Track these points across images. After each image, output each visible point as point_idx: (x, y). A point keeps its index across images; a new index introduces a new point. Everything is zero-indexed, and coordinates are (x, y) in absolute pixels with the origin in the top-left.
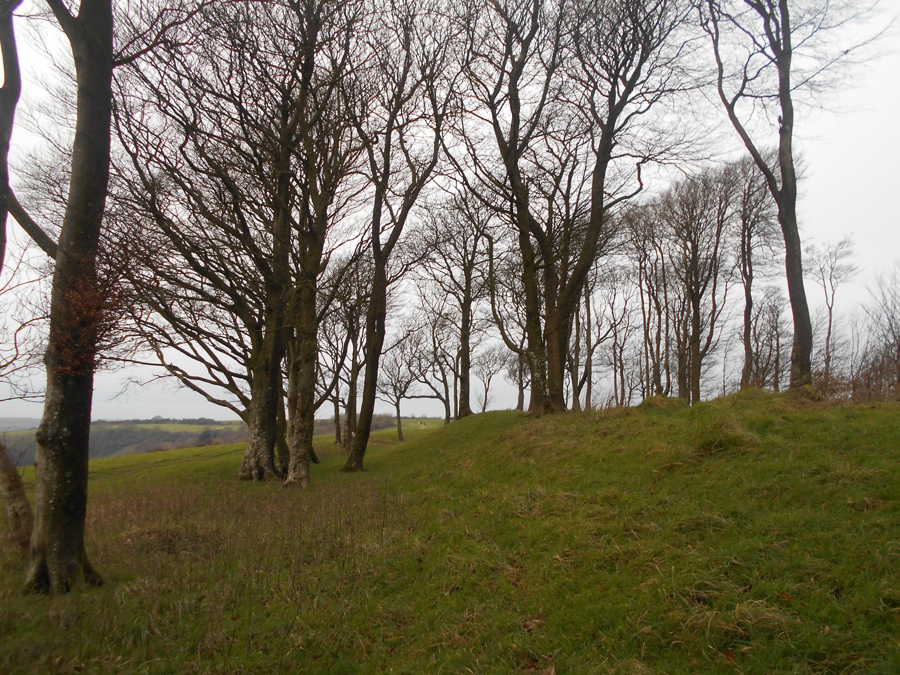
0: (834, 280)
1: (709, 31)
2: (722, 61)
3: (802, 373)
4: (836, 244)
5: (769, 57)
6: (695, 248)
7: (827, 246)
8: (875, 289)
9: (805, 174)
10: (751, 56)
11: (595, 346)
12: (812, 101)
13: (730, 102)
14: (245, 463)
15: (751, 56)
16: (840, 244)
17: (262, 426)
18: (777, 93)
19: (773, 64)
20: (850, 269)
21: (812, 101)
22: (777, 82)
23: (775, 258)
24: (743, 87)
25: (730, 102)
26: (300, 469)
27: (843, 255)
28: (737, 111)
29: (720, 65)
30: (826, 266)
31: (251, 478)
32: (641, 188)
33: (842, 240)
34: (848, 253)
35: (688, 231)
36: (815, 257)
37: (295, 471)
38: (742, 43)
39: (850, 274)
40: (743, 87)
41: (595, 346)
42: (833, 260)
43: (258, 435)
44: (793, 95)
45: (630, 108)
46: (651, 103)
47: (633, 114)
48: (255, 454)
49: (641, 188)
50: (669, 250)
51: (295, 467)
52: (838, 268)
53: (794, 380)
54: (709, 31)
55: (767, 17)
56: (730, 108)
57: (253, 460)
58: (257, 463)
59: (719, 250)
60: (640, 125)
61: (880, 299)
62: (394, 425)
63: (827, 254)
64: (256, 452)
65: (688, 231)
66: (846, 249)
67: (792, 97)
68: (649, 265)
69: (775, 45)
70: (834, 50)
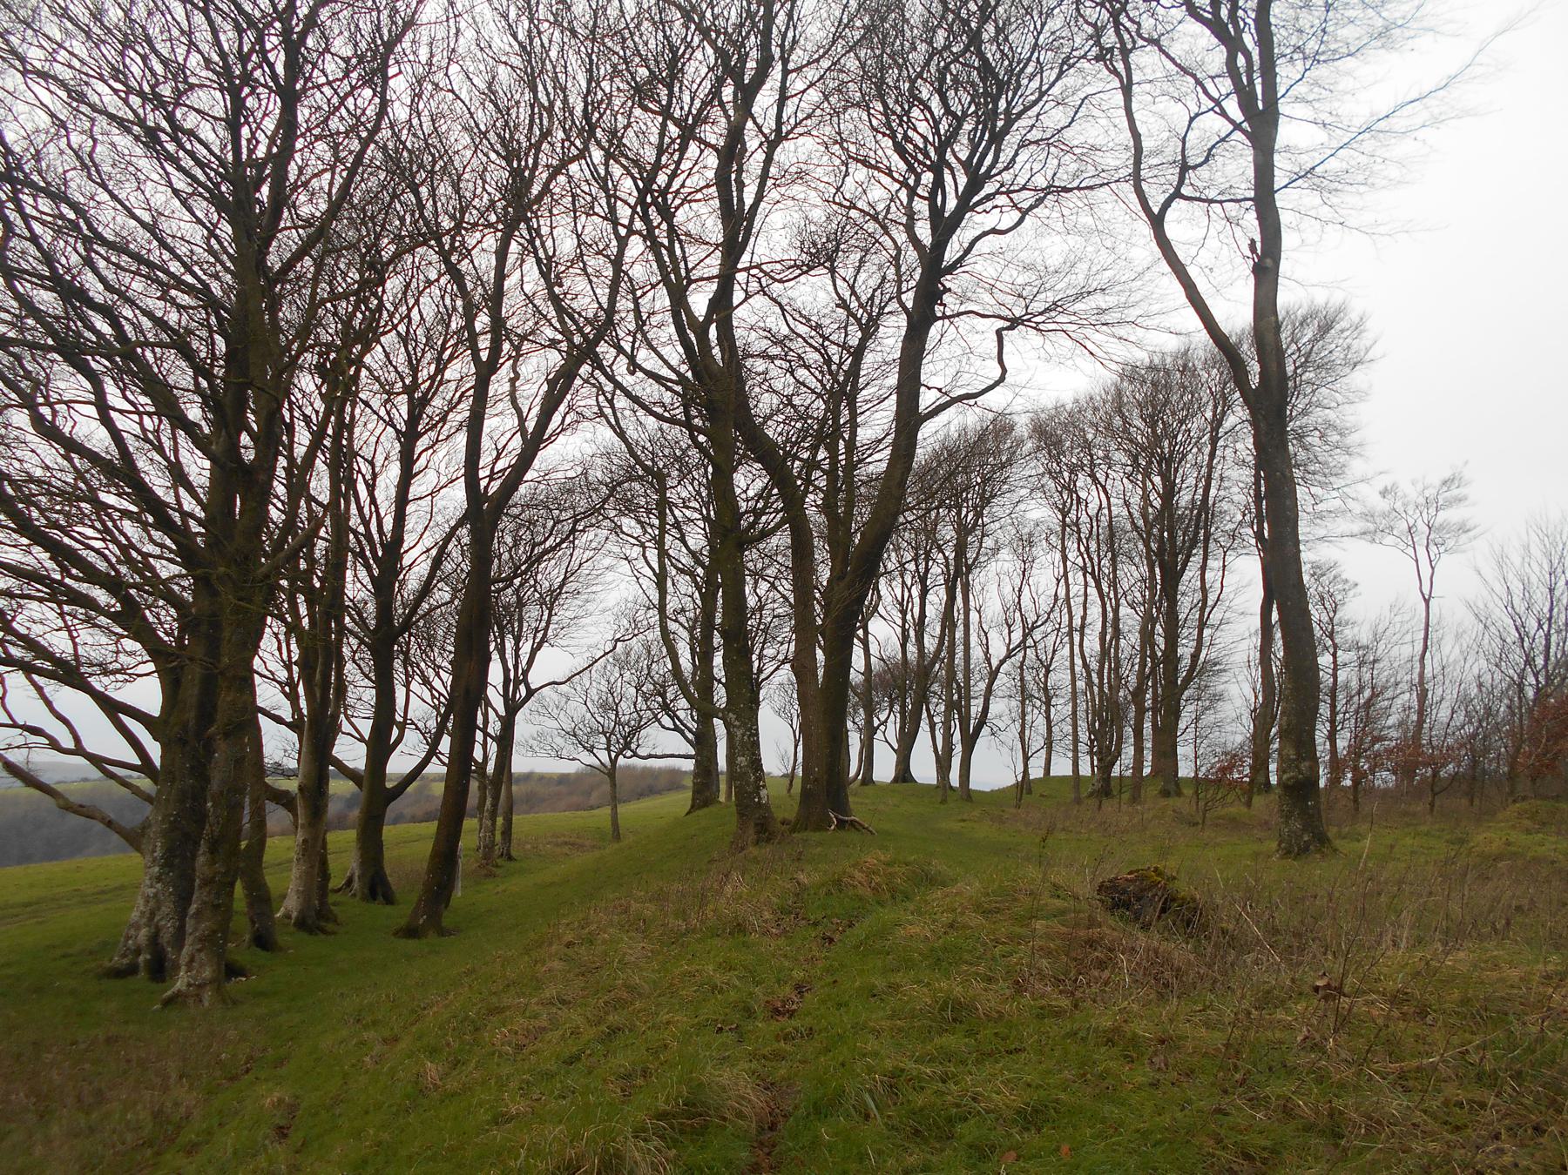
0: (1433, 548)
1: (1115, 72)
2: (1141, 129)
3: (1300, 758)
4: (1437, 483)
5: (1232, 121)
6: (1169, 492)
7: (1420, 487)
8: (1490, 572)
9: (1370, 356)
10: (1192, 120)
11: (1002, 662)
12: (1325, 212)
13: (1156, 210)
14: (128, 938)
15: (1192, 120)
16: (1445, 483)
17: (168, 862)
18: (1251, 194)
19: (1238, 135)
20: (1463, 529)
21: (1325, 212)
22: (1251, 173)
23: (1319, 508)
24: (1181, 182)
25: (1156, 210)
26: (202, 965)
27: (1450, 503)
28: (1171, 229)
29: (1136, 136)
30: (1420, 522)
31: (132, 970)
32: (1002, 379)
33: (1447, 474)
34: (1460, 500)
35: (1157, 459)
36: (1398, 506)
37: (189, 969)
38: (1175, 94)
39: (1464, 537)
40: (1181, 182)
41: (1002, 662)
42: (1432, 511)
43: (159, 879)
44: (1281, 200)
45: (975, 223)
46: (1024, 213)
47: (985, 234)
48: (151, 918)
49: (1002, 379)
50: (1117, 494)
51: (192, 960)
52: (1441, 528)
53: (1284, 772)
54: (1115, 72)
55: (1233, 44)
56: (1157, 222)
57: (144, 931)
58: (154, 939)
59: (1213, 492)
60: (1001, 253)
61: (1500, 589)
62: (684, 787)
63: (1421, 500)
64: (153, 914)
65: (1157, 459)
66: (1455, 492)
67: (1278, 204)
68: (1084, 518)
69: (1245, 96)
70: (1356, 110)
